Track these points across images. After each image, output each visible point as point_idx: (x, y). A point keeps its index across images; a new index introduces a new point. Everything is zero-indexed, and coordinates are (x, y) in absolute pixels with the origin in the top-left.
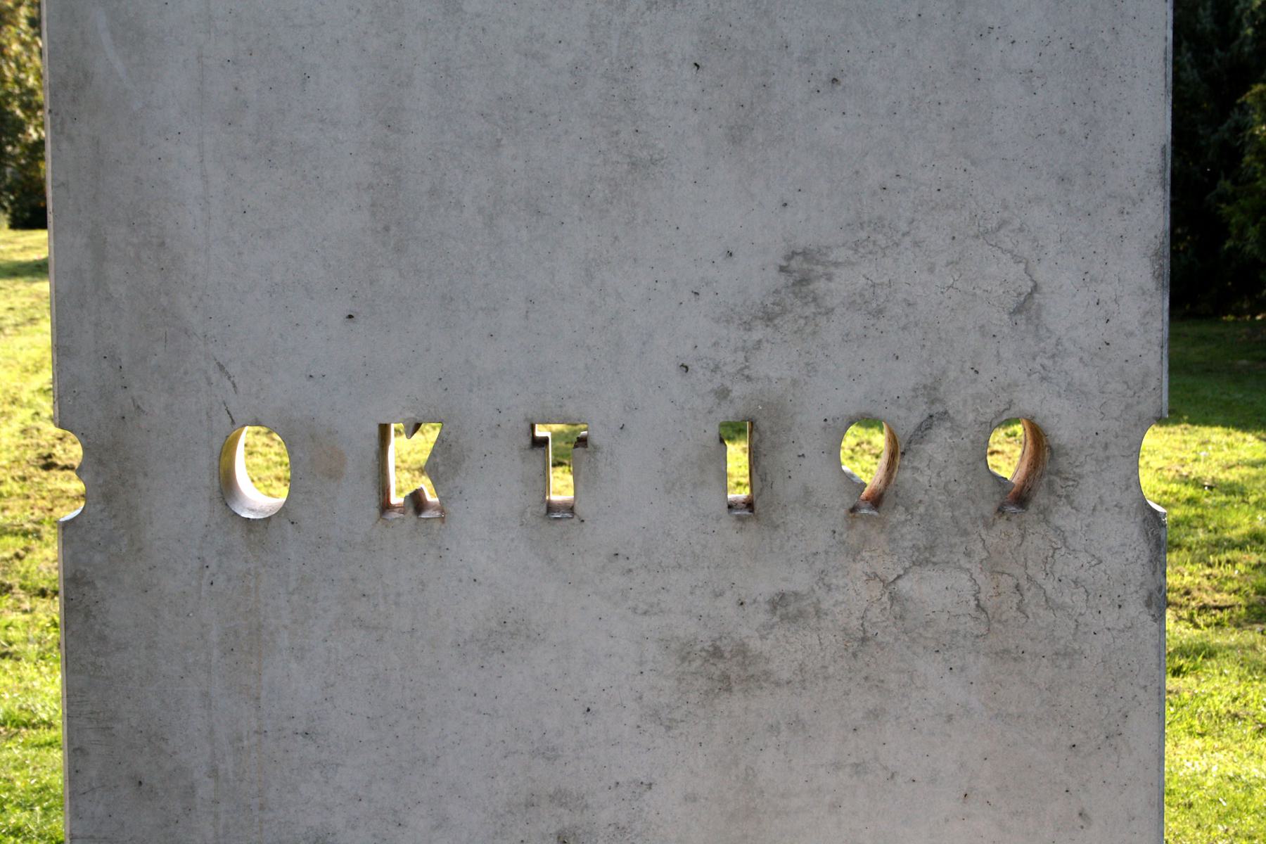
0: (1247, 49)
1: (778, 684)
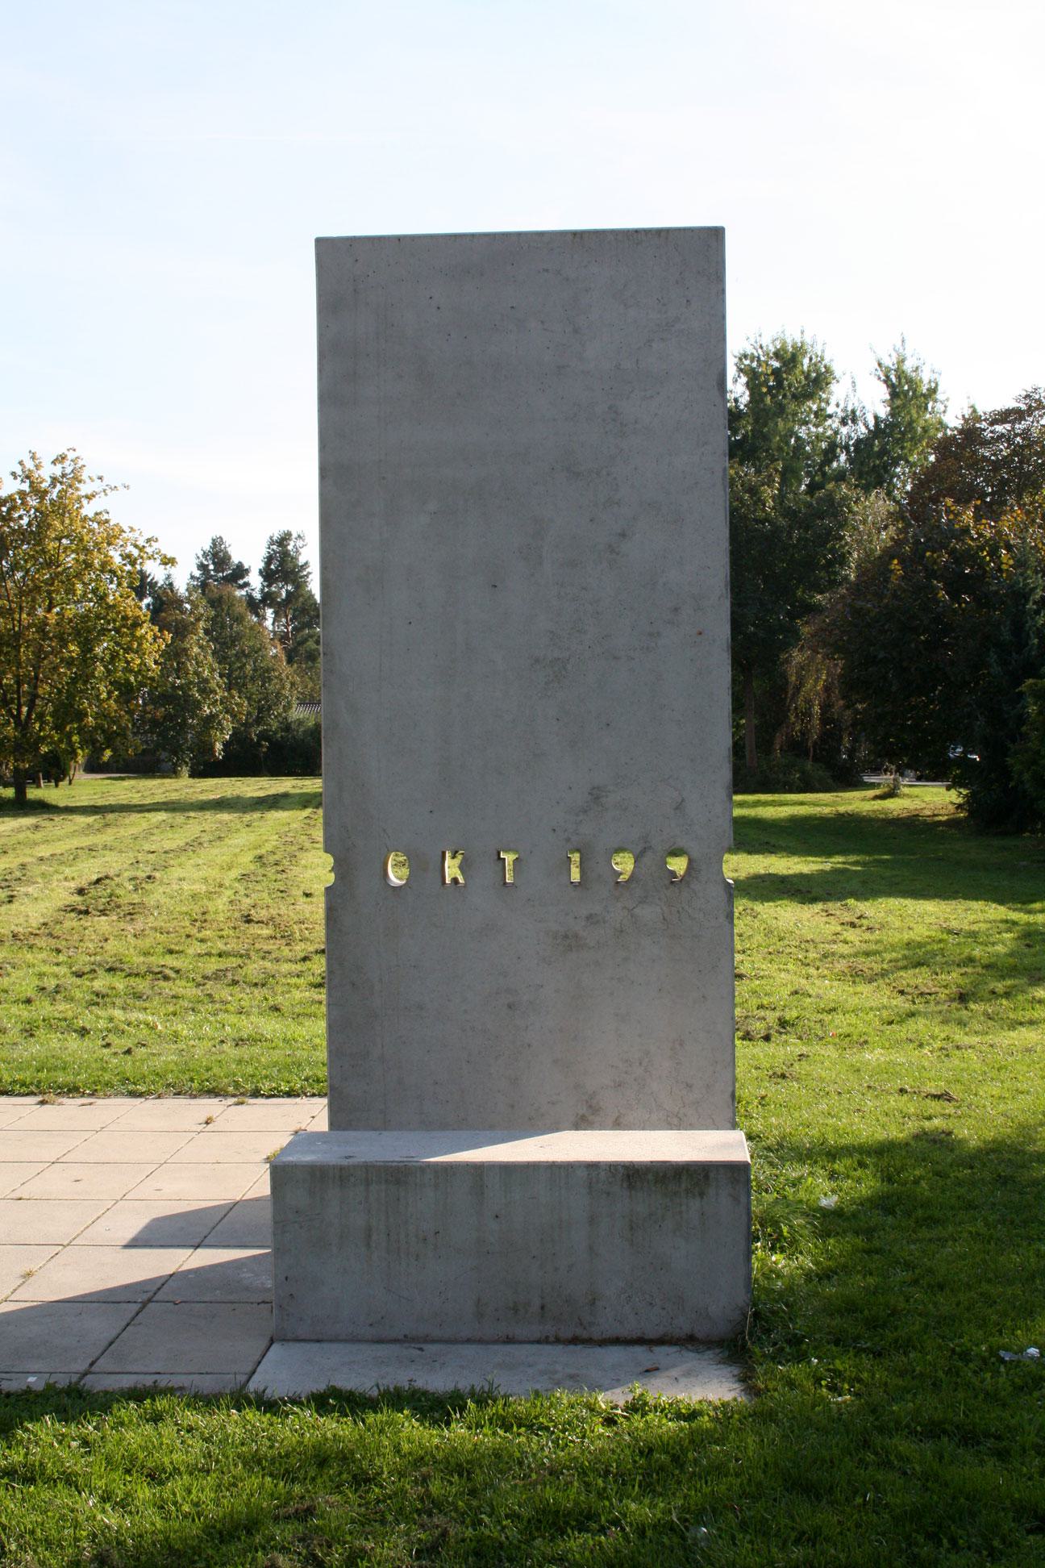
0: (1033, 653)
1: (590, 948)
